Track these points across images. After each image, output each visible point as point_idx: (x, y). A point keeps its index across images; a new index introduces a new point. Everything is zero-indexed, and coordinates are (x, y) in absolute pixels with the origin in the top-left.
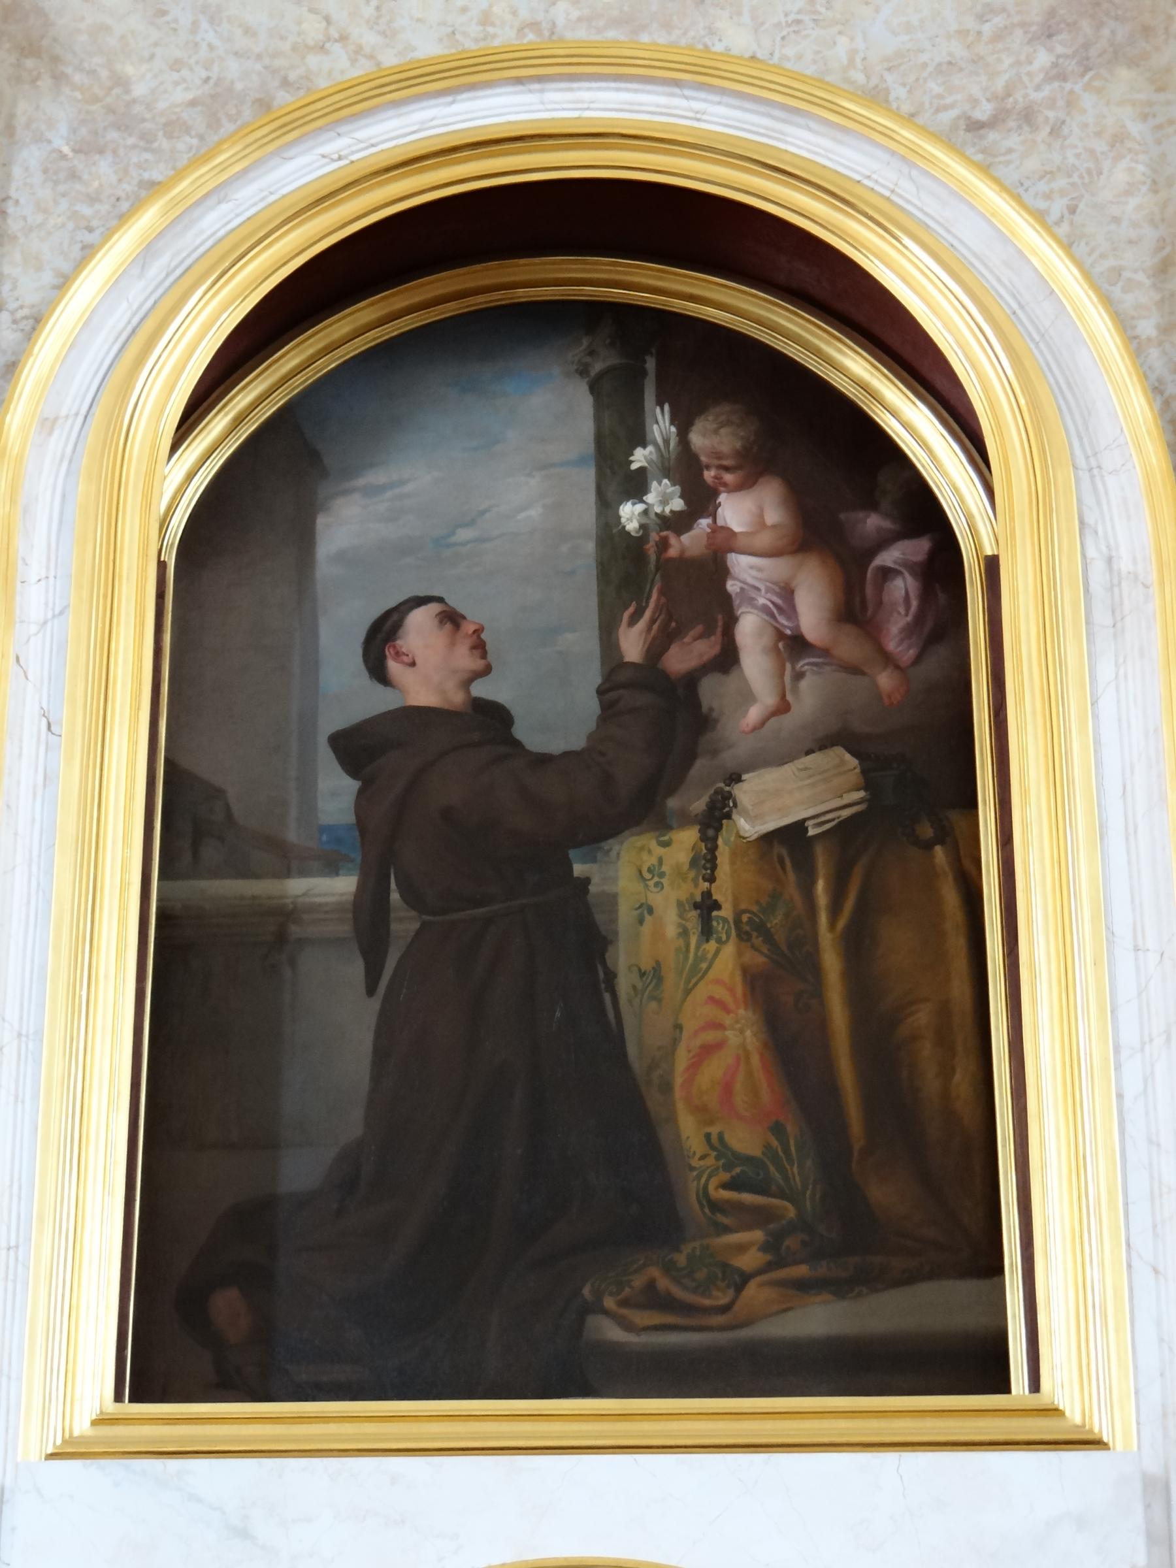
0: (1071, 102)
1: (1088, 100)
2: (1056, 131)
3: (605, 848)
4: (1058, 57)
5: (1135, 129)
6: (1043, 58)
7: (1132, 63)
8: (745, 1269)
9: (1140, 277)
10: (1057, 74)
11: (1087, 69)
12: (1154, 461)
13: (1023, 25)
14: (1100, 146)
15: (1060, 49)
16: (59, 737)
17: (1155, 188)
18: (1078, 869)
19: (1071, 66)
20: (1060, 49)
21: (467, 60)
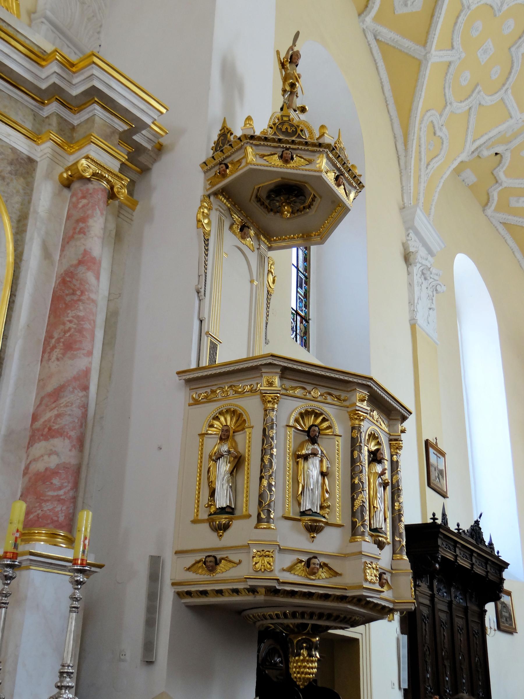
0: (12, 180)
1: (15, 181)
2: (8, 184)
3: (366, 537)
4: (12, 169)
5: (21, 191)
6: (9, 168)
7: (24, 178)
8: (291, 564)
9: (15, 221)
10: (10, 173)
11: (16, 175)
12: (11, 260)
13: (8, 160)
14: (15, 191)
15: (13, 168)
16: (172, 578)
17: (21, 205)
18: (160, 600)
19: (13, 172)
20: (13, 168)
21: (370, 695)
